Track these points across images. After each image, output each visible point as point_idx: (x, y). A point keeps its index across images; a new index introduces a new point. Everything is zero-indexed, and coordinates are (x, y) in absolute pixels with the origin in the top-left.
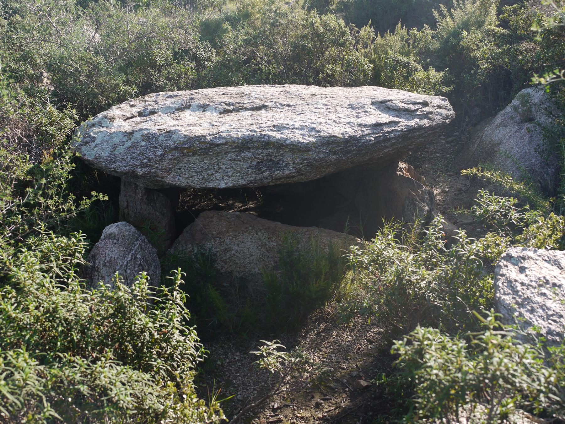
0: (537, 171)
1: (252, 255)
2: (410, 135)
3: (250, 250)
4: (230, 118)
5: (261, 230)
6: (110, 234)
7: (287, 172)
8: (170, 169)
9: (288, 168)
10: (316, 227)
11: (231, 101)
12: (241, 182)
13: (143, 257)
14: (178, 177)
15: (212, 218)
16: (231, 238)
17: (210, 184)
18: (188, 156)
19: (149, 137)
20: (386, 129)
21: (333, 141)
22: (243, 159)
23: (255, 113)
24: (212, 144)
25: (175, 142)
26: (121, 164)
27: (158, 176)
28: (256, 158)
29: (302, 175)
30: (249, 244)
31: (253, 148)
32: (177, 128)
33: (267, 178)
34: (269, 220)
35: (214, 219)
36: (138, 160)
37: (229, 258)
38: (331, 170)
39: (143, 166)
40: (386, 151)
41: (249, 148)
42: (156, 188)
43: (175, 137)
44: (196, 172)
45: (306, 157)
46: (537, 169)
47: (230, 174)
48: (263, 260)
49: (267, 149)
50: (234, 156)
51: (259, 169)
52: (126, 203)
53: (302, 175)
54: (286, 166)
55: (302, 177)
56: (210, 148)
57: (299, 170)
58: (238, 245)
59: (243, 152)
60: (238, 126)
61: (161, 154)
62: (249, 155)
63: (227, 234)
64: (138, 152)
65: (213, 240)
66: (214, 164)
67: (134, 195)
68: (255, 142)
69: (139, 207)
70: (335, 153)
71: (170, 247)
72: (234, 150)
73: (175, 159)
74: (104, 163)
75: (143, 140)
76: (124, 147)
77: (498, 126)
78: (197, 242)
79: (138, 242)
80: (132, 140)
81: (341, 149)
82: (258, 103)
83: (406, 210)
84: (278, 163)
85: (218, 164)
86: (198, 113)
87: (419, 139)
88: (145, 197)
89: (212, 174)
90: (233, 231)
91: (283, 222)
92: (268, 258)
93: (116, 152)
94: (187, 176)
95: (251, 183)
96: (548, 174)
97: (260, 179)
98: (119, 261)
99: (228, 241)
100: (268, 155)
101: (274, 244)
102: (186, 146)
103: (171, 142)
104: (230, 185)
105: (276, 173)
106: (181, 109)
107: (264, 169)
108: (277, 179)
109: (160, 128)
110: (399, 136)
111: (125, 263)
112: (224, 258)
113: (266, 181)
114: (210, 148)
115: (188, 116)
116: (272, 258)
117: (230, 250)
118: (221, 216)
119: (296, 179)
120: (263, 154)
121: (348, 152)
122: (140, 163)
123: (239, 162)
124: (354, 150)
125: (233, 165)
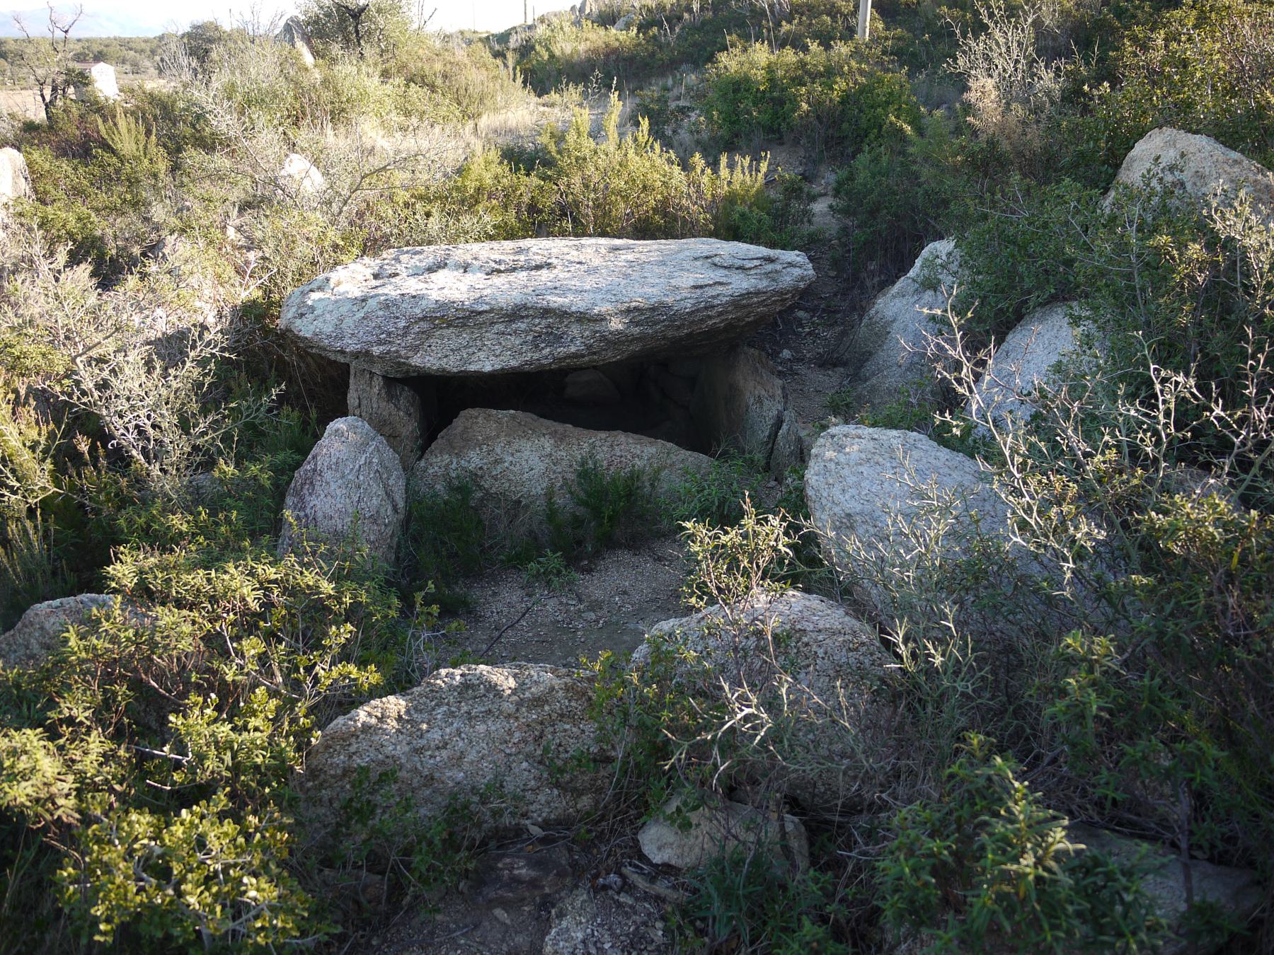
4: (498, 280)
6: (337, 431)
7: (573, 349)
8: (417, 346)
9: (575, 343)
11: (502, 257)
12: (514, 363)
13: (381, 463)
19: (387, 305)
20: (711, 292)
23: (533, 273)
27: (400, 356)
29: (595, 353)
30: (527, 453)
31: (527, 316)
32: (424, 292)
35: (480, 420)
38: (636, 347)
39: (380, 343)
41: (523, 317)
42: (398, 376)
43: (424, 302)
50: (501, 327)
51: (537, 346)
53: (595, 353)
56: (469, 317)
57: (589, 347)
60: (506, 290)
62: (523, 326)
69: (375, 406)
70: (637, 324)
71: (420, 459)
82: (539, 259)
86: (456, 273)
91: (576, 425)
99: (498, 450)
100: (548, 326)
103: (418, 311)
104: (498, 367)
106: (431, 270)
110: (727, 302)
113: (544, 362)
114: (469, 317)
115: (441, 277)
117: (501, 461)
120: (541, 324)
121: (655, 323)
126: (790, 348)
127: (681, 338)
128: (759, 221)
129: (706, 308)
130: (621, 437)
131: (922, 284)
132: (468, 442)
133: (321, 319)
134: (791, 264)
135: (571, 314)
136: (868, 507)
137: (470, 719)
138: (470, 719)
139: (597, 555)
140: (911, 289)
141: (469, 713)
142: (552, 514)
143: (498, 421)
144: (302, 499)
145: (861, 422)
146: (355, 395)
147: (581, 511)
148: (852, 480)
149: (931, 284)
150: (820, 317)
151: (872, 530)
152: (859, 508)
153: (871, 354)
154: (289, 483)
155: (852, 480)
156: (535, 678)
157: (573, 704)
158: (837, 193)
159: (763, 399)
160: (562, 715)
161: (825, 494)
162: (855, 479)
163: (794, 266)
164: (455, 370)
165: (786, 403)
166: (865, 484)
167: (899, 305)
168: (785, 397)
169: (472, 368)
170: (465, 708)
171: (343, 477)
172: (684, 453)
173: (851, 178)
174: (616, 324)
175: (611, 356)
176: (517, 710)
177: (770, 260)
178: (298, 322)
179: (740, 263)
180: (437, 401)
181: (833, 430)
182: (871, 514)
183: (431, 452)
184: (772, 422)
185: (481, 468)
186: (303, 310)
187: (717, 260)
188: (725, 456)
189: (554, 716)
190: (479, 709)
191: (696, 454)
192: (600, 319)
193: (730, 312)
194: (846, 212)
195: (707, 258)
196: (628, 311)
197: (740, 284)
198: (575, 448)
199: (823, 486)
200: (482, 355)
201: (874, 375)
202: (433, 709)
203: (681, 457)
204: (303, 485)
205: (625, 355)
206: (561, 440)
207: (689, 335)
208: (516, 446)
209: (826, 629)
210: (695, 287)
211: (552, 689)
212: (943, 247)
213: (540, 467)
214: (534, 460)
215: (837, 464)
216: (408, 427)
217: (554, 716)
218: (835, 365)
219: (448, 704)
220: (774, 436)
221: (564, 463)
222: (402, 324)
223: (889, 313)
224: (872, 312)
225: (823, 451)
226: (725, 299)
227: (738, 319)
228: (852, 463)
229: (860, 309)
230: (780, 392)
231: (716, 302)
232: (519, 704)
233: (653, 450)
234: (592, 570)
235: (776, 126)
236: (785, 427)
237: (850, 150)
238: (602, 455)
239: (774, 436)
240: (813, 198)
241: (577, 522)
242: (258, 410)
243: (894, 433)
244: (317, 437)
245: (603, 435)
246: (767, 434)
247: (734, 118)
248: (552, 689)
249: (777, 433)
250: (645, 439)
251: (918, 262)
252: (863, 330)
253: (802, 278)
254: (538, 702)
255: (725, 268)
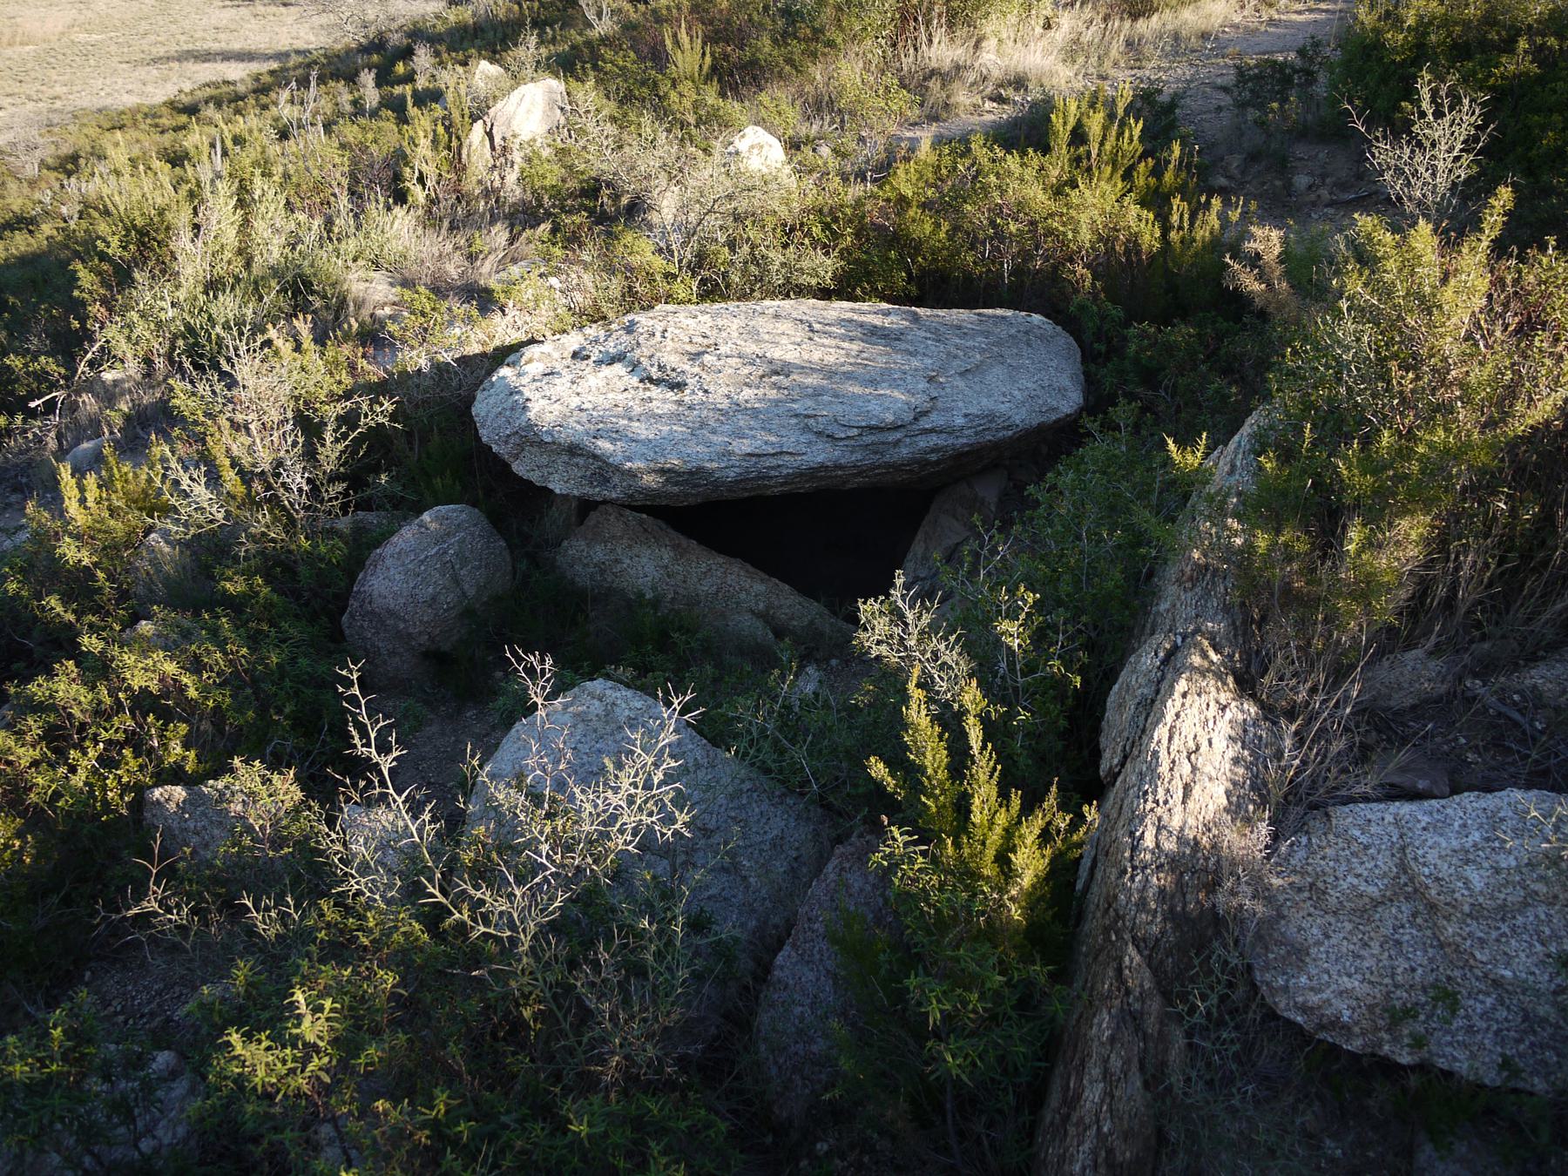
7: (614, 495)
20: (773, 462)
35: (612, 518)
91: (700, 542)
99: (619, 551)
174: (650, 480)
208: (636, 550)
214: (650, 568)
233: (762, 588)
245: (721, 559)
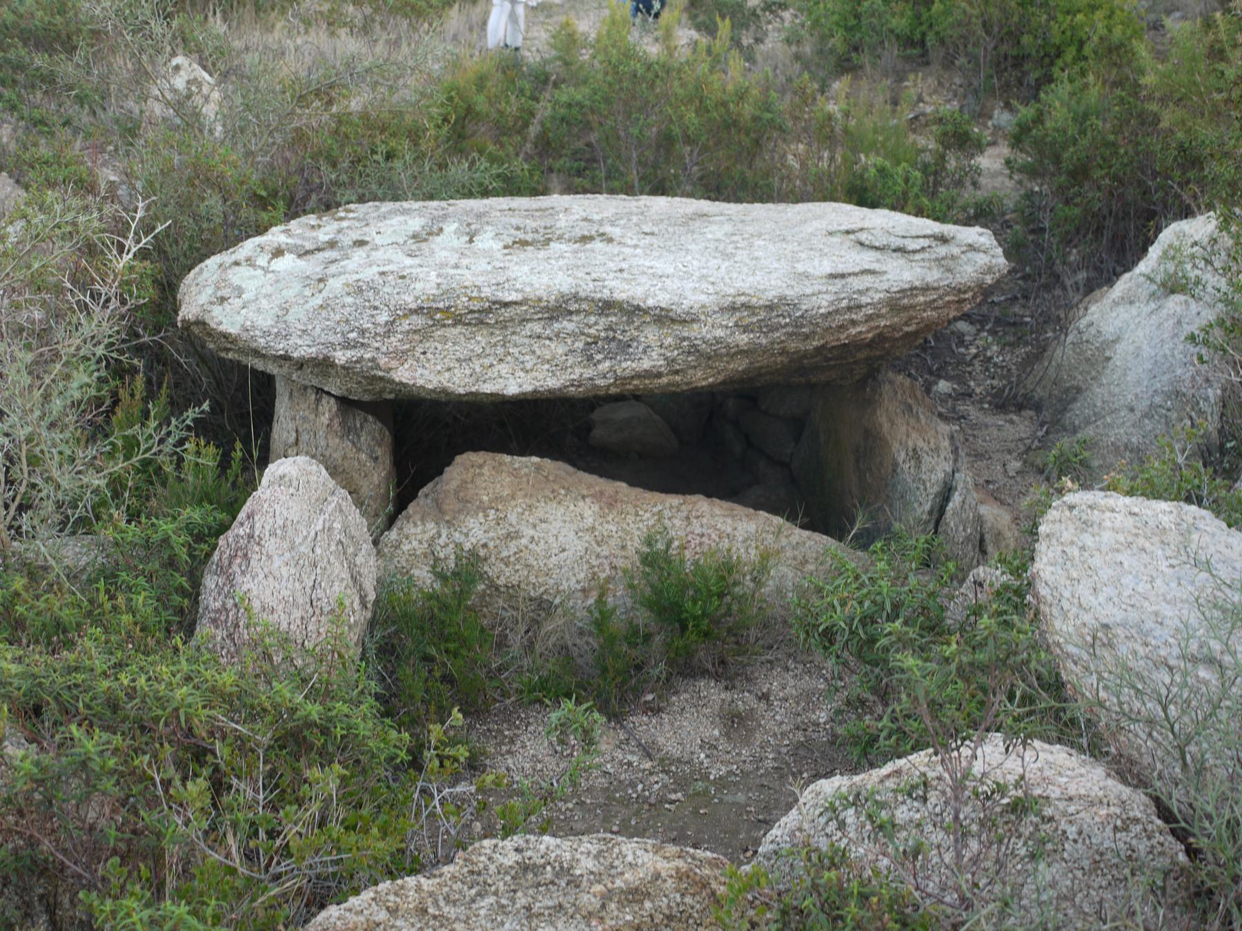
0: (1184, 395)
1: (564, 550)
2: (906, 301)
3: (560, 538)
5: (583, 497)
7: (646, 364)
9: (650, 356)
10: (701, 497)
13: (345, 530)
14: (420, 371)
15: (481, 466)
16: (520, 510)
17: (486, 386)
18: (444, 326)
20: (857, 283)
21: (743, 305)
22: (557, 336)
24: (494, 303)
25: (417, 298)
26: (300, 342)
27: (378, 367)
28: (583, 334)
29: (677, 372)
30: (558, 524)
31: (578, 312)
33: (605, 377)
34: (601, 476)
35: (485, 470)
36: (336, 333)
37: (515, 553)
38: (740, 365)
39: (347, 345)
40: (853, 331)
41: (571, 313)
42: (367, 398)
44: (458, 360)
45: (686, 334)
46: (1184, 390)
47: (528, 366)
48: (588, 562)
49: (607, 316)
50: (537, 328)
52: (294, 435)
53: (677, 372)
54: (645, 352)
55: (678, 378)
56: (489, 311)
57: (671, 361)
58: (534, 526)
59: (557, 320)
60: (542, 275)
61: (387, 323)
63: (513, 503)
64: (338, 317)
65: (481, 515)
66: (495, 345)
67: (312, 417)
68: (581, 300)
70: (746, 329)
72: (540, 316)
73: (415, 332)
74: (262, 340)
75: (349, 294)
76: (307, 306)
77: (1116, 303)
78: (447, 518)
79: (336, 499)
80: (325, 294)
81: (759, 321)
83: (899, 470)
84: (629, 346)
85: (504, 345)
87: (924, 311)
88: (336, 422)
89: (491, 365)
90: (526, 496)
91: (632, 483)
92: (598, 556)
93: (289, 318)
94: (439, 368)
95: (572, 385)
96: (1206, 399)
97: (591, 379)
98: (301, 527)
99: (513, 518)
100: (609, 328)
101: (611, 527)
102: (441, 305)
103: (409, 299)
104: (528, 388)
105: (624, 365)
107: (599, 357)
108: (625, 378)
109: (382, 269)
111: (313, 534)
112: (505, 554)
113: (601, 382)
114: (489, 311)
116: (606, 557)
118: (501, 464)
119: (665, 380)
122: (341, 340)
123: (547, 342)
124: (787, 325)
125: (536, 347)
126: (947, 378)
127: (805, 355)
128: (907, 180)
129: (849, 309)
130: (702, 505)
131: (1163, 285)
132: (466, 504)
133: (253, 307)
134: (972, 248)
135: (646, 311)
136: (1133, 616)
137: (529, 918)
138: (529, 918)
139: (667, 686)
140: (1144, 293)
141: (528, 909)
142: (601, 619)
143: (515, 473)
144: (230, 580)
145: (1112, 487)
146: (291, 426)
147: (643, 617)
148: (1106, 573)
149: (1173, 286)
150: (993, 332)
151: (1141, 651)
152: (1119, 616)
153: (1079, 390)
154: (209, 555)
155: (1106, 573)
156: (630, 858)
157: (688, 900)
158: (1017, 141)
159: (923, 452)
160: (670, 918)
161: (1067, 594)
162: (1110, 572)
163: (978, 253)
164: (462, 391)
165: (956, 461)
166: (1127, 580)
167: (1126, 316)
168: (955, 451)
169: (488, 388)
170: (522, 901)
171: (292, 548)
172: (799, 534)
173: (1039, 119)
175: (702, 378)
176: (603, 906)
177: (943, 240)
178: (217, 311)
179: (899, 242)
180: (419, 439)
181: (1069, 498)
182: (1139, 626)
183: (408, 518)
184: (936, 489)
185: (485, 546)
186: (225, 292)
187: (863, 237)
188: (864, 541)
189: (658, 918)
190: (544, 902)
191: (817, 536)
192: (688, 320)
193: (883, 316)
194: (1032, 172)
195: (848, 232)
196: (733, 308)
197: (901, 274)
198: (630, 519)
199: (1063, 581)
200: (504, 369)
201: (1088, 422)
202: (473, 901)
203: (794, 539)
204: (232, 558)
205: (720, 378)
206: (611, 506)
207: (818, 350)
208: (540, 513)
209: (1080, 797)
210: (833, 276)
211: (657, 876)
212: (1201, 227)
213: (576, 546)
215: (1083, 548)
216: (376, 475)
217: (658, 918)
218: (1020, 408)
219: (496, 893)
220: (939, 511)
221: (612, 542)
222: (383, 318)
223: (1109, 330)
224: (1083, 323)
225: (1055, 523)
226: (877, 296)
227: (893, 327)
228: (1104, 548)
229: (1057, 320)
230: (946, 443)
231: (865, 300)
232: (607, 897)
233: (752, 527)
234: (660, 710)
235: (917, 36)
236: (956, 498)
237: (1033, 76)
238: (677, 527)
239: (939, 511)
240: (980, 147)
241: (637, 637)
242: (161, 441)
243: (1163, 505)
244: (251, 485)
245: (675, 500)
246: (927, 507)
247: (852, 22)
248: (657, 876)
249: (942, 511)
250: (739, 509)
251: (1154, 252)
252: (1063, 353)
253: (990, 270)
254: (635, 895)
255: (877, 248)
